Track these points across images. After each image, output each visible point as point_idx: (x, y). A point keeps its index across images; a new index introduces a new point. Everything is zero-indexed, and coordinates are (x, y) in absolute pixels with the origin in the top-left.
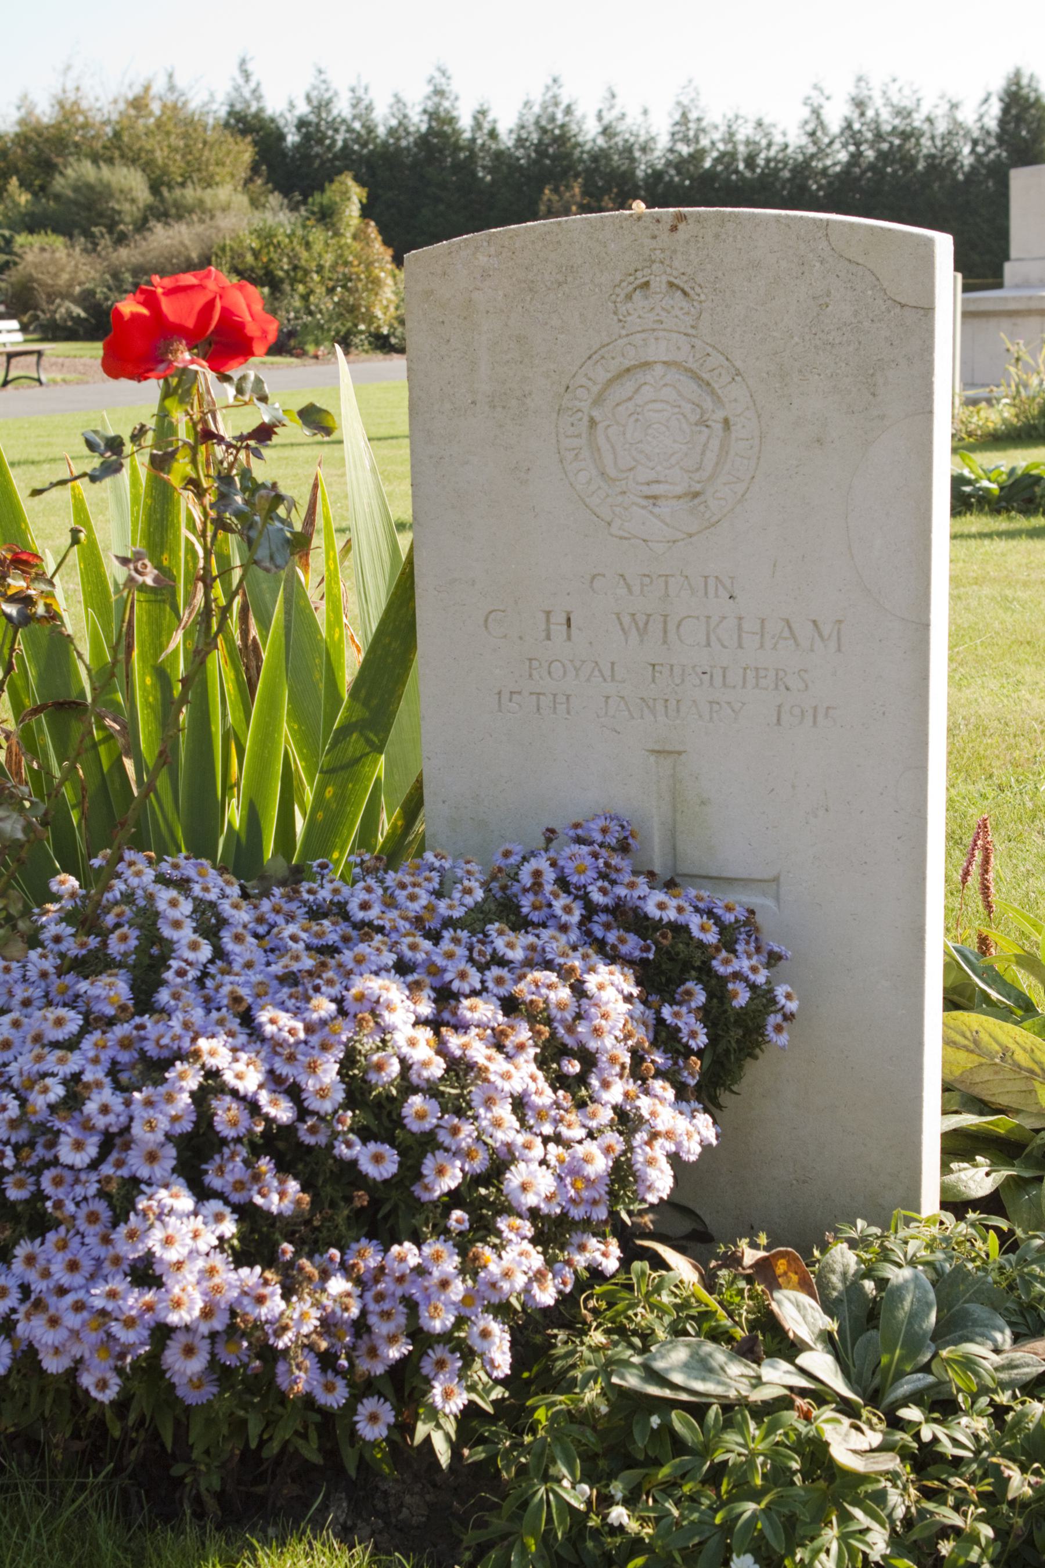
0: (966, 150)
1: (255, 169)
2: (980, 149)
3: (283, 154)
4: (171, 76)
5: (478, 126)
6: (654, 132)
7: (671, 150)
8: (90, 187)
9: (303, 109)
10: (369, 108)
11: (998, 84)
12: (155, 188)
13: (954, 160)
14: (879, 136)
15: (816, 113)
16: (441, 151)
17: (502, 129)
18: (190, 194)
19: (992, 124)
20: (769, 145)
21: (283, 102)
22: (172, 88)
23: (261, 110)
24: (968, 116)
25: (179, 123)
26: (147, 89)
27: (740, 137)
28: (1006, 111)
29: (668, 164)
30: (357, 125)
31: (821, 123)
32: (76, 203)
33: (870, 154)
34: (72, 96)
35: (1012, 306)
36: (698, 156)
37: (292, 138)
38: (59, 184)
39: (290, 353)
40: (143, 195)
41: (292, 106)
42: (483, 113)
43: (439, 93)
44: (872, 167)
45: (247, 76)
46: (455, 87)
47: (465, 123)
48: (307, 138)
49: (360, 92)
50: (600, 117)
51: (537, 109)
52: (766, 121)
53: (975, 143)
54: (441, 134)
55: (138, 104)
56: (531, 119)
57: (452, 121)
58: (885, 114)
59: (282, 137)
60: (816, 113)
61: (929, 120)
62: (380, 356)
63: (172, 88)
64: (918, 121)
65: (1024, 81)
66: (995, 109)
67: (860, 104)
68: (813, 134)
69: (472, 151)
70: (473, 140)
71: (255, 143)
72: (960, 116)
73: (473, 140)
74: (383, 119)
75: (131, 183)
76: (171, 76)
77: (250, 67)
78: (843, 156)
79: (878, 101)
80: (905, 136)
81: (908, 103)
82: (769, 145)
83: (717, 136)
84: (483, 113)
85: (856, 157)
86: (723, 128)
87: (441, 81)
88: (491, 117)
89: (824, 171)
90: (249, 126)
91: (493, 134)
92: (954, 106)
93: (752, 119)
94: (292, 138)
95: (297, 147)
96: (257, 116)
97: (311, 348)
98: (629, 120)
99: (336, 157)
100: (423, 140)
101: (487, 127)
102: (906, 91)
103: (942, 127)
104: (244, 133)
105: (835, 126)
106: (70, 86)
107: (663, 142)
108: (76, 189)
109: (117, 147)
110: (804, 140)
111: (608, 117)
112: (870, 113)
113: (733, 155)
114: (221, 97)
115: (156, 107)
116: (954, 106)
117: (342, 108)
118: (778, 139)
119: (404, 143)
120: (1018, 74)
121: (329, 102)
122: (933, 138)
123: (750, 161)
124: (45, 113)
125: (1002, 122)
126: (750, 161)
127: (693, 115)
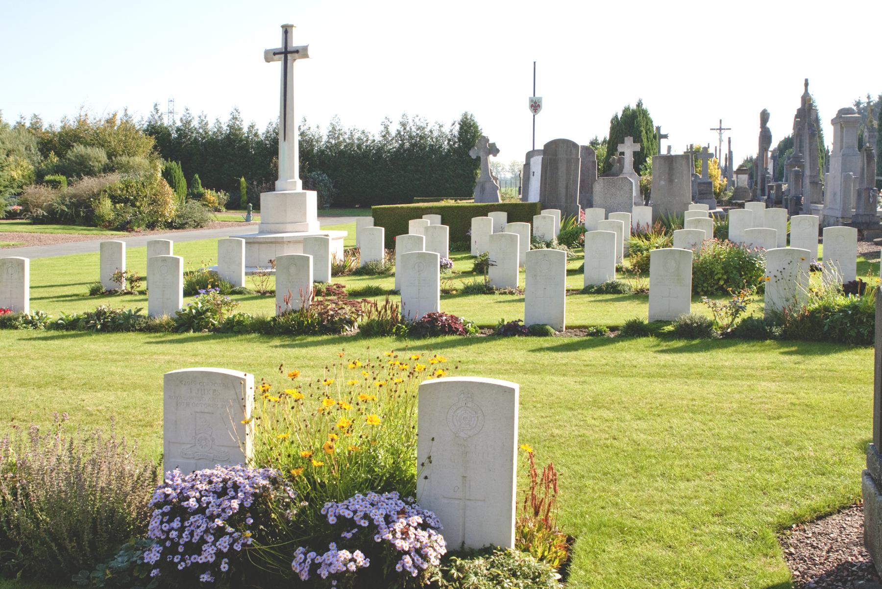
0: (446, 143)
1: (155, 147)
2: (451, 143)
3: (170, 141)
4: (126, 110)
5: (250, 131)
6: (321, 134)
7: (328, 142)
8: (82, 156)
9: (179, 124)
10: (206, 124)
11: (459, 118)
12: (109, 156)
13: (441, 147)
14: (411, 137)
15: (386, 128)
16: (234, 141)
17: (260, 133)
18: (124, 159)
19: (456, 132)
20: (367, 140)
21: (171, 120)
22: (126, 115)
23: (163, 124)
24: (446, 130)
25: (127, 128)
26: (115, 115)
27: (356, 137)
28: (461, 128)
29: (327, 147)
30: (201, 131)
31: (388, 133)
32: (76, 162)
33: (407, 145)
34: (83, 118)
35: (261, 240)
36: (340, 143)
37: (174, 135)
38: (70, 154)
39: (127, 230)
40: (104, 158)
41: (174, 122)
42: (252, 127)
43: (235, 118)
44: (408, 149)
45: (157, 111)
46: (242, 116)
47: (245, 130)
48: (180, 135)
49: (203, 118)
50: (300, 129)
51: (274, 126)
52: (366, 131)
53: (449, 140)
54: (235, 135)
55: (110, 122)
56: (271, 129)
57: (240, 129)
58: (414, 129)
59: (170, 135)
60: (386, 128)
61: (431, 131)
62: (167, 230)
63: (126, 115)
64: (427, 131)
65: (469, 117)
66: (457, 127)
67: (404, 125)
68: (384, 136)
69: (247, 141)
70: (248, 137)
71: (156, 138)
72: (443, 130)
73: (248, 137)
74: (211, 127)
75: (100, 155)
76: (126, 110)
77: (158, 107)
78: (397, 145)
79: (411, 124)
80: (421, 138)
81: (424, 125)
82: (367, 140)
83: (346, 136)
84: (252, 127)
85: (402, 145)
86: (349, 133)
87: (236, 114)
88: (256, 128)
89: (389, 151)
90: (156, 131)
91: (256, 135)
92: (441, 126)
93: (361, 130)
94: (174, 135)
95: (177, 138)
96: (160, 126)
97: (136, 228)
98: (311, 130)
99: (191, 143)
100: (228, 137)
101: (254, 132)
102: (422, 120)
103: (435, 134)
104: (151, 135)
105: (393, 133)
106: (83, 114)
107: (325, 139)
108: (76, 157)
109: (97, 139)
110: (381, 139)
111: (302, 129)
112: (408, 129)
113: (352, 144)
114: (146, 119)
115: (118, 122)
116: (441, 126)
117: (195, 123)
118: (371, 138)
119: (220, 138)
120: (465, 115)
121: (190, 121)
122: (432, 138)
123: (359, 146)
124: (72, 124)
125: (460, 133)
126: (359, 146)
127: (337, 129)
